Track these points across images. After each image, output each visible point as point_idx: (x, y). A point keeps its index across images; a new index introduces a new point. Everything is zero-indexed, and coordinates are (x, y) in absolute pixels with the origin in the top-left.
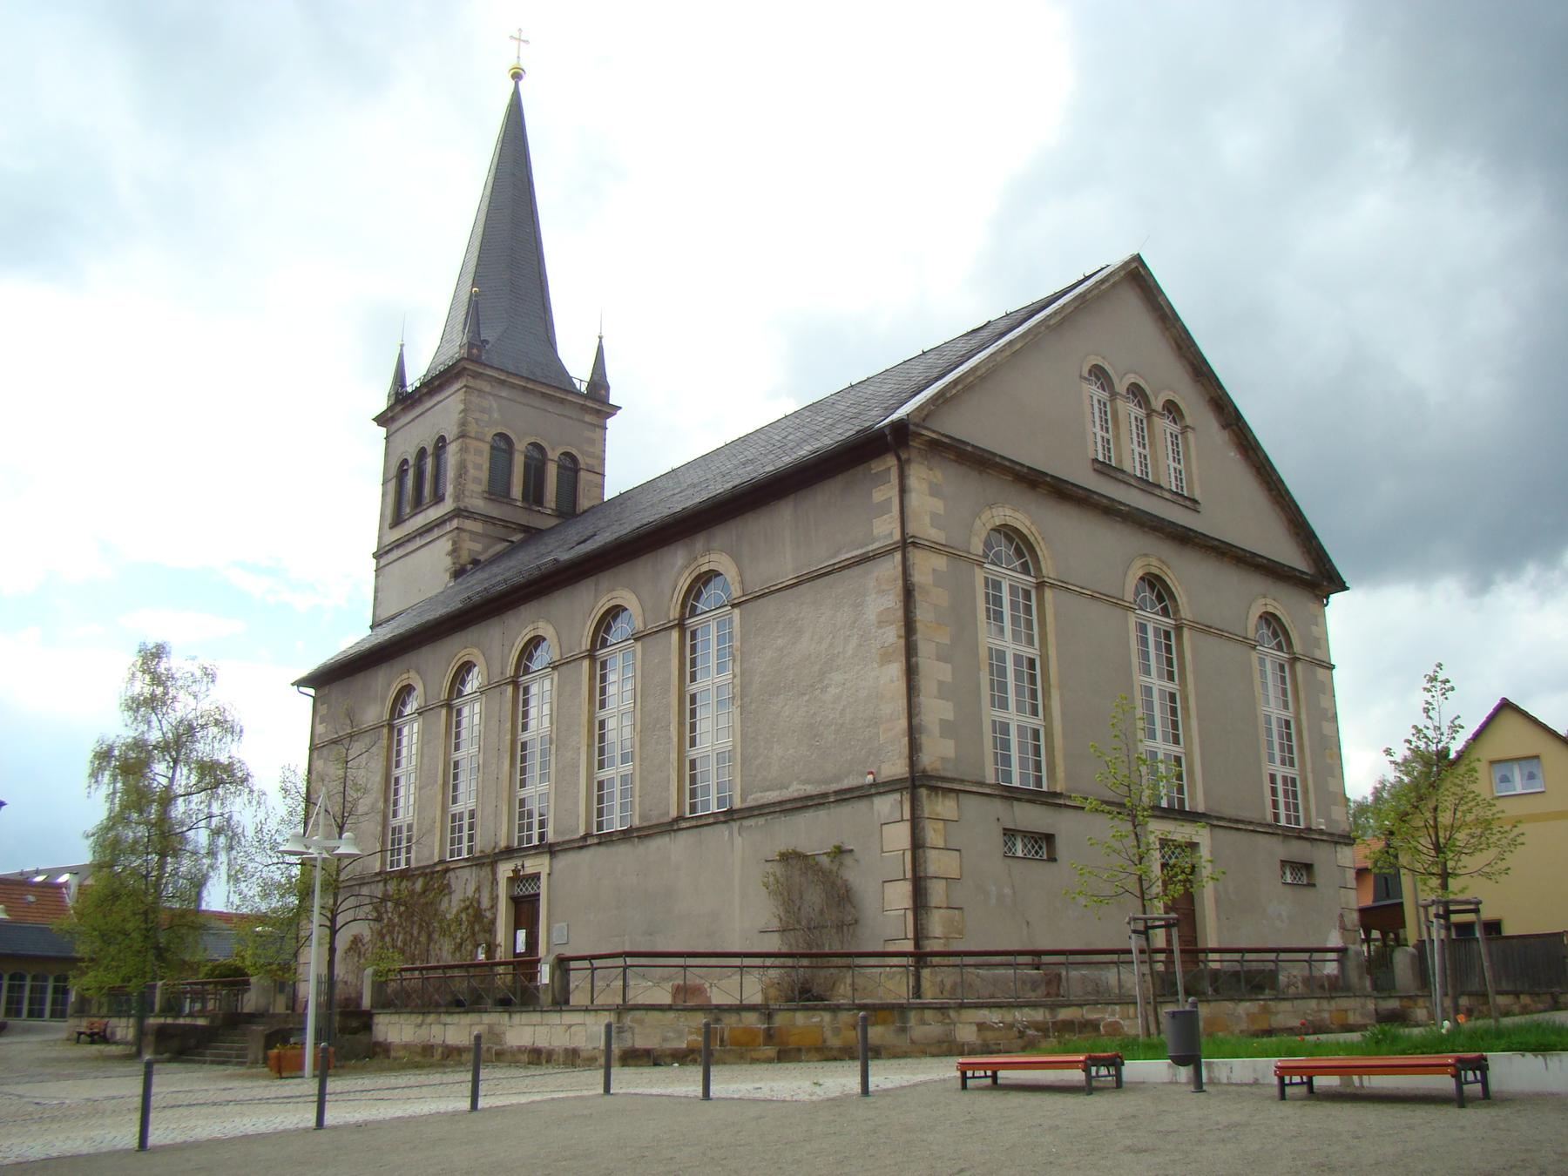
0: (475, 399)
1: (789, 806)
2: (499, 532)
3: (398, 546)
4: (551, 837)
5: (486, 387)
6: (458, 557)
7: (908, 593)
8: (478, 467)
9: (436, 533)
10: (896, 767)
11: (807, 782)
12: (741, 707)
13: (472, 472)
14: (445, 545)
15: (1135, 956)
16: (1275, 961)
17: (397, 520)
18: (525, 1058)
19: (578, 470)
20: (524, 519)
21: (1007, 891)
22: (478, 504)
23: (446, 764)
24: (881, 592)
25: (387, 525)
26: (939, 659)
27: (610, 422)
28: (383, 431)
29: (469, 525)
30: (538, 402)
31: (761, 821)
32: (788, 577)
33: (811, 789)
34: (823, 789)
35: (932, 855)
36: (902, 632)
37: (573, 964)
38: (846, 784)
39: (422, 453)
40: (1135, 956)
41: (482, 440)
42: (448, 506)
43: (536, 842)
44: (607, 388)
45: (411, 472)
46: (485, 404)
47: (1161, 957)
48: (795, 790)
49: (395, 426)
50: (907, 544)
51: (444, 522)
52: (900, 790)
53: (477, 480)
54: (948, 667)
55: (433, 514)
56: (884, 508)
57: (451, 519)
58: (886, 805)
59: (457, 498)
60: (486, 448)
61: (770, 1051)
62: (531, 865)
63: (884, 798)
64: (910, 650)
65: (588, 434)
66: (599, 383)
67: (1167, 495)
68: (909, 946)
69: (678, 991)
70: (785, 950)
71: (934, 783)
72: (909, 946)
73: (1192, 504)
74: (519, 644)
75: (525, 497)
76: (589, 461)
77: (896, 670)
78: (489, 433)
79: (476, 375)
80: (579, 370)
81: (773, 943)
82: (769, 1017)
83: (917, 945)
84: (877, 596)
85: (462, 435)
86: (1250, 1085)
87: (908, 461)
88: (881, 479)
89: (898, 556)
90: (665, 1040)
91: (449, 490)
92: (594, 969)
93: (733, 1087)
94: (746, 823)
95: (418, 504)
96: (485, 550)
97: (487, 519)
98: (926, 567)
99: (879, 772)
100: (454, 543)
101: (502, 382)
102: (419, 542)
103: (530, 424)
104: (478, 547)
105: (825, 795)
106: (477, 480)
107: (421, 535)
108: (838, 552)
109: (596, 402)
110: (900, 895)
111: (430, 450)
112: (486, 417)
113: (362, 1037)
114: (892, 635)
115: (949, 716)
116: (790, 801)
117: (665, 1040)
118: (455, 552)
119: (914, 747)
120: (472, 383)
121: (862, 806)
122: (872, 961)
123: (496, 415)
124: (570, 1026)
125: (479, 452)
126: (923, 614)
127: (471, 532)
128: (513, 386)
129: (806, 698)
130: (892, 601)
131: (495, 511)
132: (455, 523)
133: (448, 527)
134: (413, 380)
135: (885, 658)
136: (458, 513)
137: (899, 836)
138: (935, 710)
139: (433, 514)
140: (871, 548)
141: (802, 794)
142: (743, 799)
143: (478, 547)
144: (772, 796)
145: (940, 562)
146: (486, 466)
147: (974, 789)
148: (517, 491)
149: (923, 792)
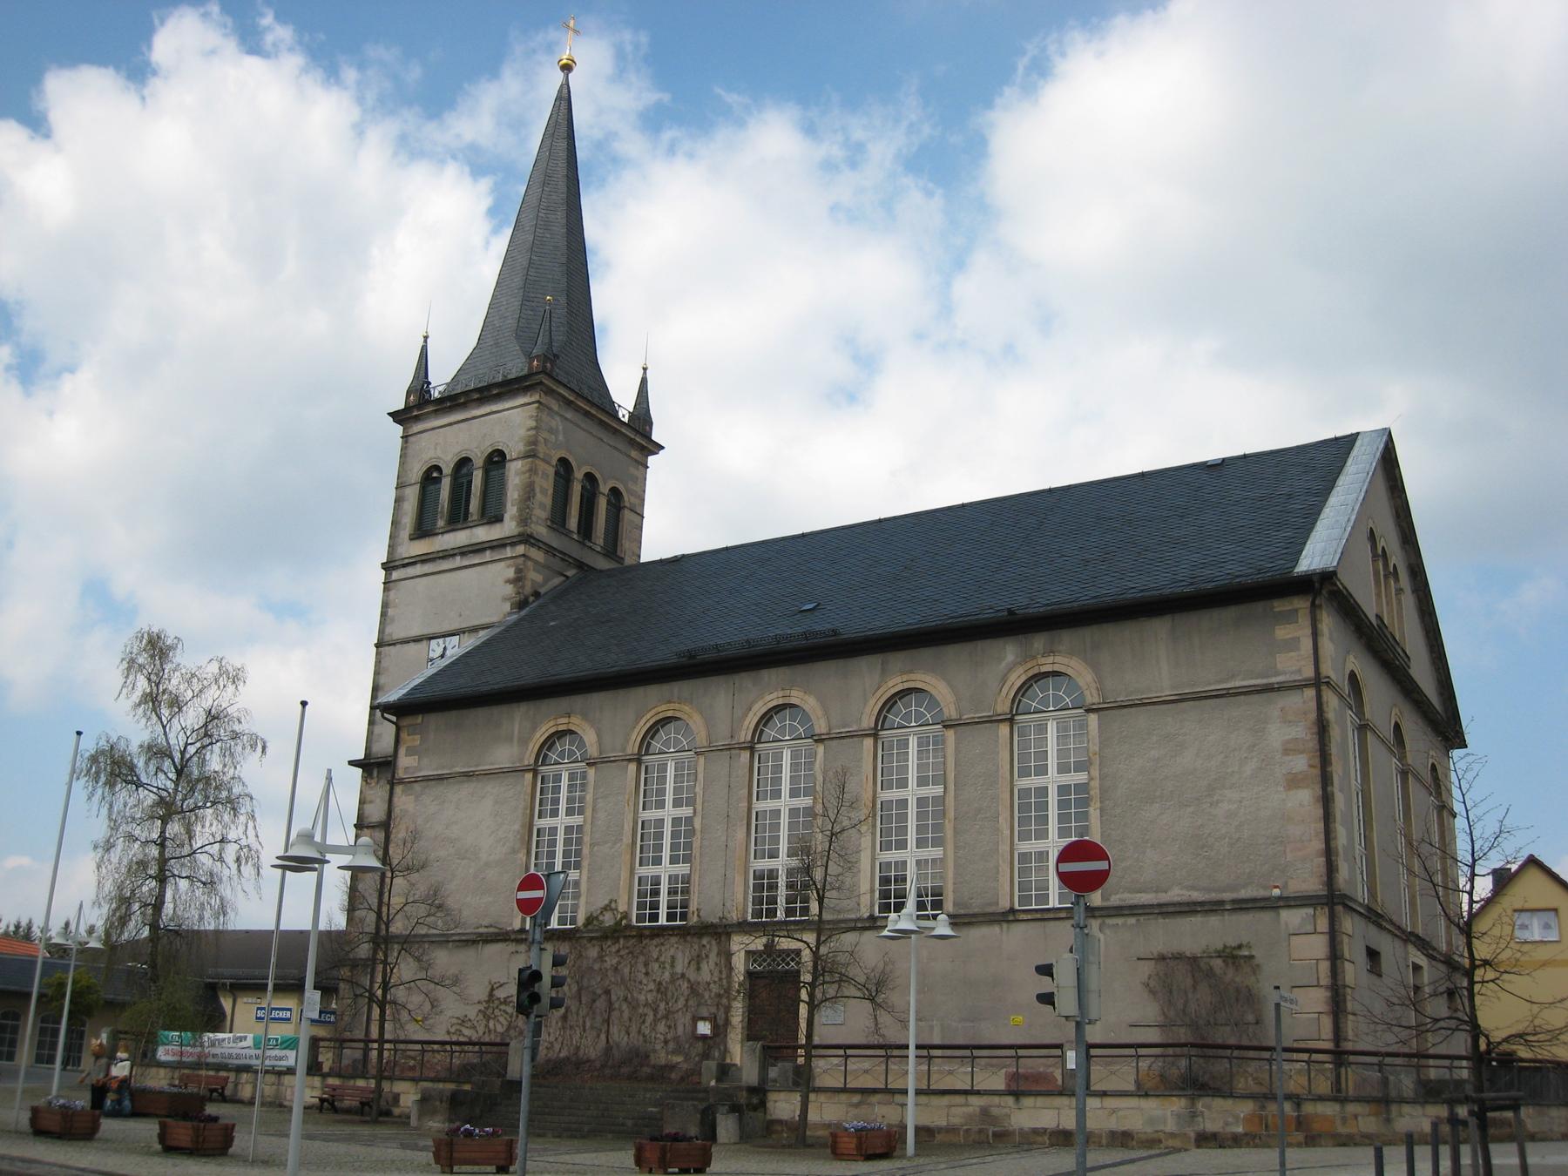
0: (544, 416)
1: (1171, 909)
2: (556, 563)
3: (423, 562)
5: (555, 406)
6: (523, 587)
8: (543, 491)
9: (488, 556)
10: (1308, 881)
11: (1193, 888)
12: (1102, 810)
13: (539, 496)
15: (912, 1051)
17: (422, 530)
18: (849, 1144)
19: (623, 509)
20: (576, 551)
22: (541, 531)
23: (635, 823)
25: (405, 533)
27: (652, 460)
28: (399, 429)
29: (535, 553)
30: (596, 430)
31: (1132, 921)
32: (1167, 693)
33: (1197, 896)
34: (1214, 896)
36: (1317, 761)
37: (1093, 1052)
39: (464, 462)
40: (912, 1051)
41: (548, 463)
42: (508, 527)
44: (651, 424)
45: (446, 484)
46: (553, 424)
47: (376, 1045)
48: (1176, 894)
49: (417, 428)
51: (504, 546)
52: (1314, 906)
53: (542, 506)
55: (483, 534)
57: (513, 544)
60: (551, 471)
61: (1300, 1137)
63: (1294, 911)
65: (632, 470)
66: (642, 417)
68: (1329, 1045)
69: (1014, 1077)
70: (1191, 1040)
74: (760, 709)
76: (633, 500)
78: (556, 455)
79: (550, 392)
80: (624, 399)
81: (1153, 1036)
82: (1298, 1105)
83: (1337, 1045)
85: (531, 455)
87: (1320, 606)
88: (1290, 617)
90: (1227, 1124)
91: (511, 511)
92: (930, 1058)
94: (1110, 921)
95: (458, 518)
96: (546, 581)
97: (550, 550)
99: (1286, 885)
100: (518, 571)
101: (569, 403)
102: (458, 561)
103: (590, 453)
104: (539, 578)
105: (1222, 902)
106: (542, 506)
107: (463, 554)
108: (1233, 677)
109: (638, 436)
110: (1314, 1001)
111: (479, 461)
113: (760, 1115)
116: (1174, 904)
117: (1227, 1124)
118: (518, 580)
119: (1331, 868)
120: (546, 400)
121: (1266, 916)
122: (1251, 1054)
123: (561, 437)
124: (1114, 1111)
125: (545, 475)
127: (536, 562)
128: (577, 409)
129: (1191, 809)
130: (1302, 731)
131: (555, 541)
132: (521, 549)
133: (509, 552)
134: (440, 378)
135: (1293, 782)
136: (526, 539)
137: (1317, 946)
139: (483, 534)
140: (1273, 680)
141: (1185, 899)
143: (539, 578)
146: (550, 491)
148: (573, 523)
149: (1339, 908)
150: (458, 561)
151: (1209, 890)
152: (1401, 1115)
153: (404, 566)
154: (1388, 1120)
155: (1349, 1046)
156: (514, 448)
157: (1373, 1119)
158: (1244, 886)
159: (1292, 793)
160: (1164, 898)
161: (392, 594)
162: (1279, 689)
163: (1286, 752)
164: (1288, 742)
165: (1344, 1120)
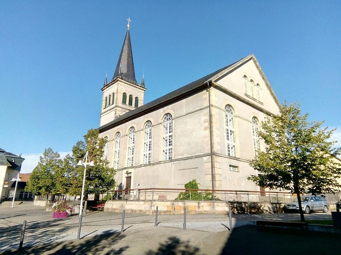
1: (184, 159)
4: (134, 165)
7: (211, 116)
9: (112, 110)
10: (208, 150)
11: (188, 154)
14: (114, 112)
16: (284, 195)
21: (230, 178)
24: (204, 116)
26: (217, 130)
29: (118, 109)
33: (189, 156)
35: (216, 169)
37: (141, 191)
38: (197, 154)
42: (114, 105)
43: (131, 166)
48: (185, 156)
50: (210, 106)
51: (114, 108)
54: (219, 131)
56: (205, 99)
58: (205, 159)
59: (116, 103)
62: (130, 171)
64: (211, 127)
67: (258, 101)
68: (211, 189)
69: (160, 197)
71: (216, 154)
72: (211, 189)
73: (262, 104)
75: (129, 104)
77: (208, 132)
84: (204, 117)
85: (117, 92)
86: (212, 214)
89: (209, 108)
92: (146, 192)
93: (197, 224)
98: (214, 111)
100: (116, 112)
108: (195, 108)
112: (122, 89)
114: (207, 124)
115: (219, 141)
126: (214, 120)
130: (207, 117)
132: (116, 108)
133: (114, 109)
135: (205, 129)
136: (116, 106)
138: (216, 140)
142: (174, 158)
143: (120, 113)
144: (180, 157)
145: (217, 110)
147: (224, 156)
150: (109, 112)
151: (191, 154)
152: (218, 206)
153: (103, 114)
154: (214, 207)
155: (216, 189)
156: (115, 92)
157: (209, 207)
158: (197, 153)
159: (206, 131)
160: (184, 157)
161: (333, 149)
162: (203, 109)
163: (204, 122)
164: (205, 120)
165: (199, 207)
